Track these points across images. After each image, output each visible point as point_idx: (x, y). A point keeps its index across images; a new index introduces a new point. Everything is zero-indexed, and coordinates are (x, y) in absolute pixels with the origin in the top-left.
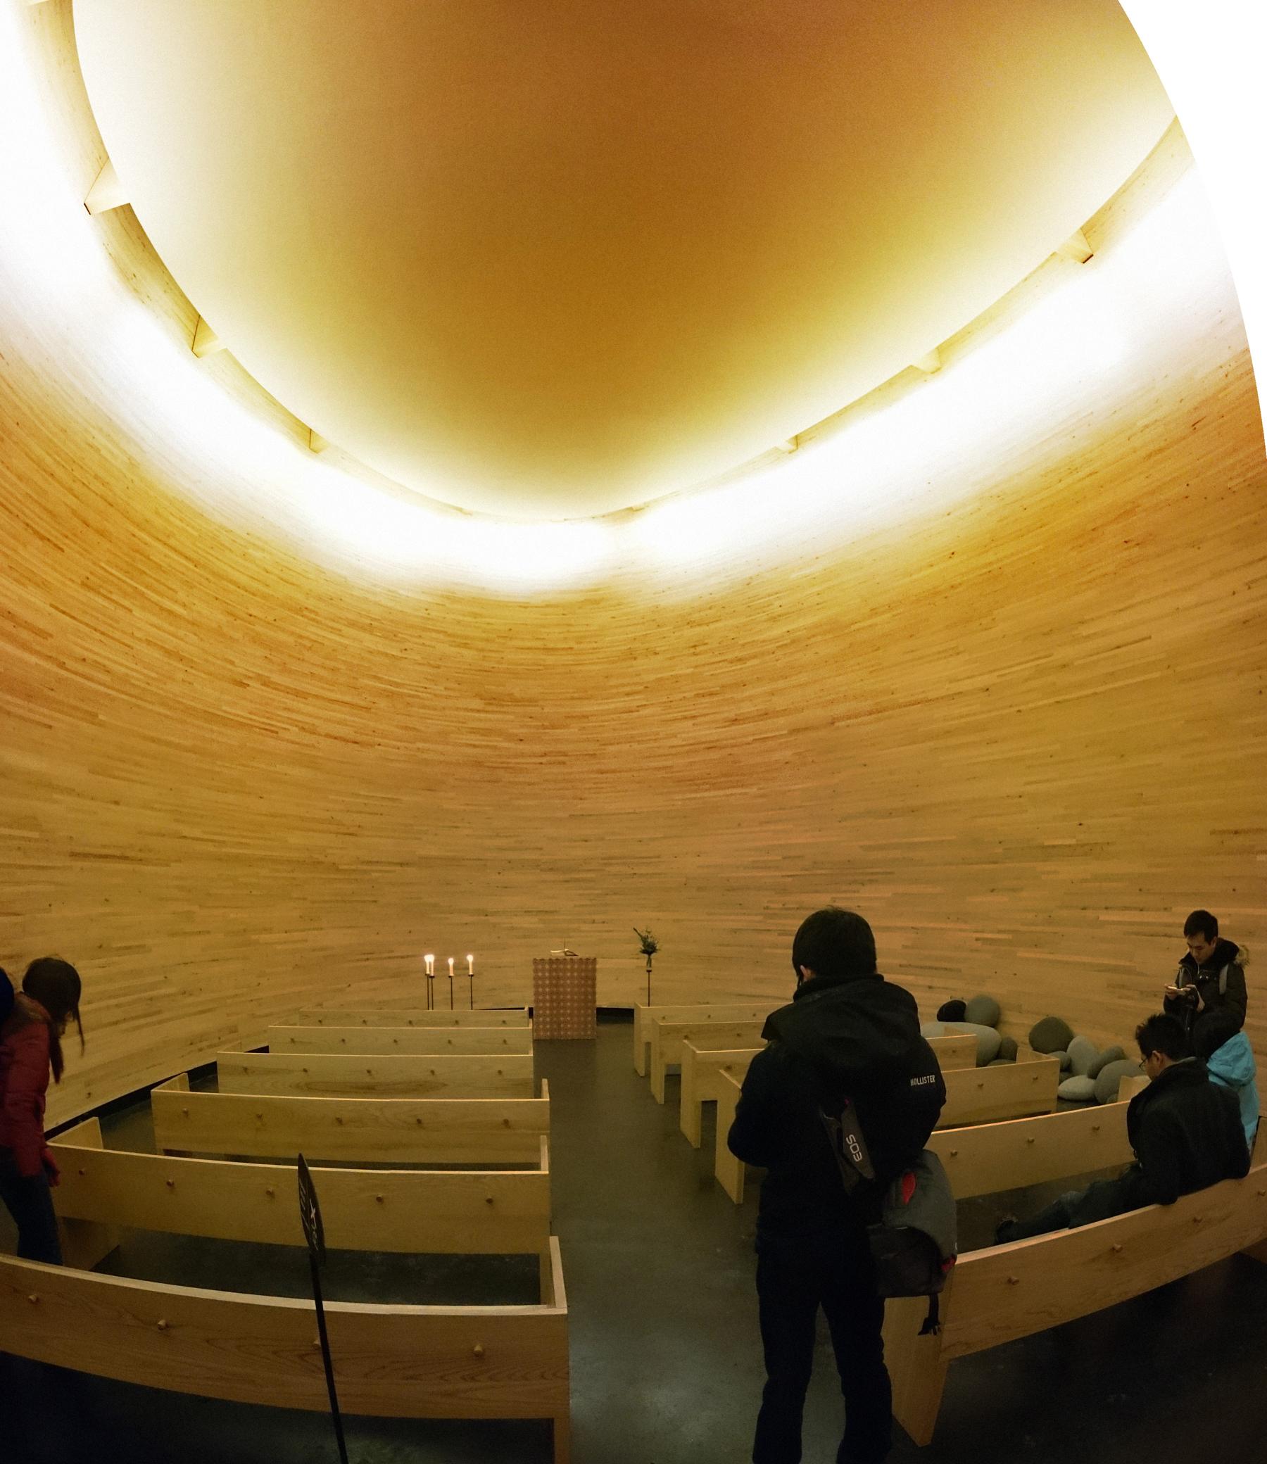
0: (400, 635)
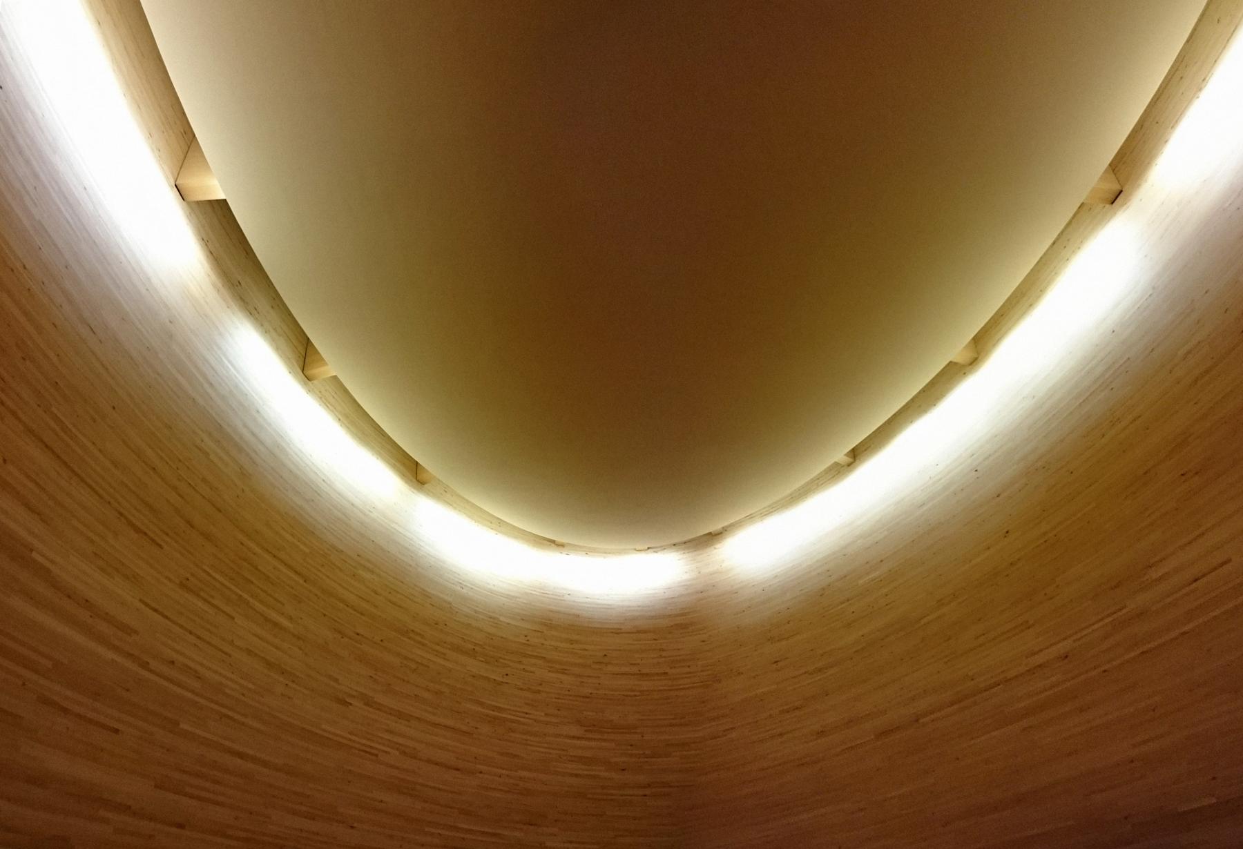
0: (501, 660)
